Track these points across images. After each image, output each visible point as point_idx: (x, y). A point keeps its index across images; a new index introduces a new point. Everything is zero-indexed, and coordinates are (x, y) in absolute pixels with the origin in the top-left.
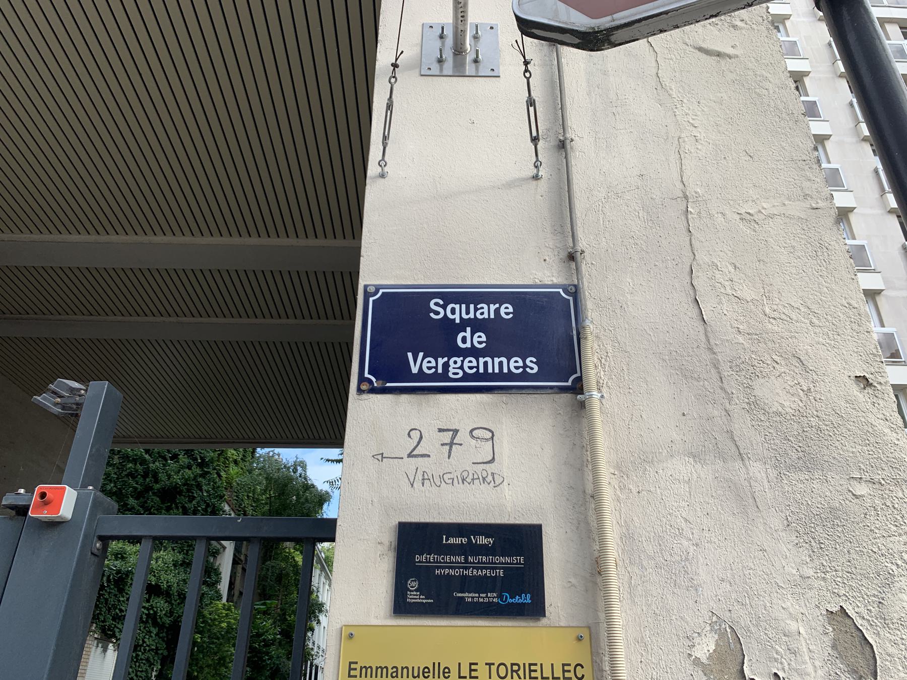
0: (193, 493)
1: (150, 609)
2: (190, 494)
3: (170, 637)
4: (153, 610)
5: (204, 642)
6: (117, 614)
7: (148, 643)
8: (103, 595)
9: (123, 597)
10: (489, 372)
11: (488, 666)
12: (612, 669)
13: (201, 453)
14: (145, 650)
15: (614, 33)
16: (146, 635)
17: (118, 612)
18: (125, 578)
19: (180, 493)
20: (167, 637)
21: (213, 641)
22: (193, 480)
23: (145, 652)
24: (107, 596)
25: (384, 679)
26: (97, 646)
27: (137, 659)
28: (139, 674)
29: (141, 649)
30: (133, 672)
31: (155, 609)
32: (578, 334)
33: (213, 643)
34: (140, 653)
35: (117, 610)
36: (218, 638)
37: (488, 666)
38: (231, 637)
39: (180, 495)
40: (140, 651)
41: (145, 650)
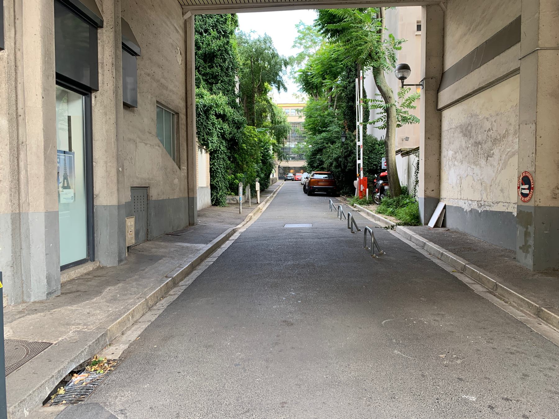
0: (224, 56)
2: (223, 57)
4: (223, 130)
5: (248, 149)
6: (208, 132)
7: (222, 149)
11: (404, 87)
12: (389, 51)
13: (222, 28)
14: (221, 153)
18: (353, 105)
19: (216, 56)
20: (228, 146)
22: (223, 47)
24: (202, 121)
27: (218, 158)
28: (220, 166)
30: (217, 165)
31: (224, 130)
35: (207, 130)
36: (255, 147)
37: (404, 87)
39: (217, 58)
40: (219, 153)
41: (221, 153)
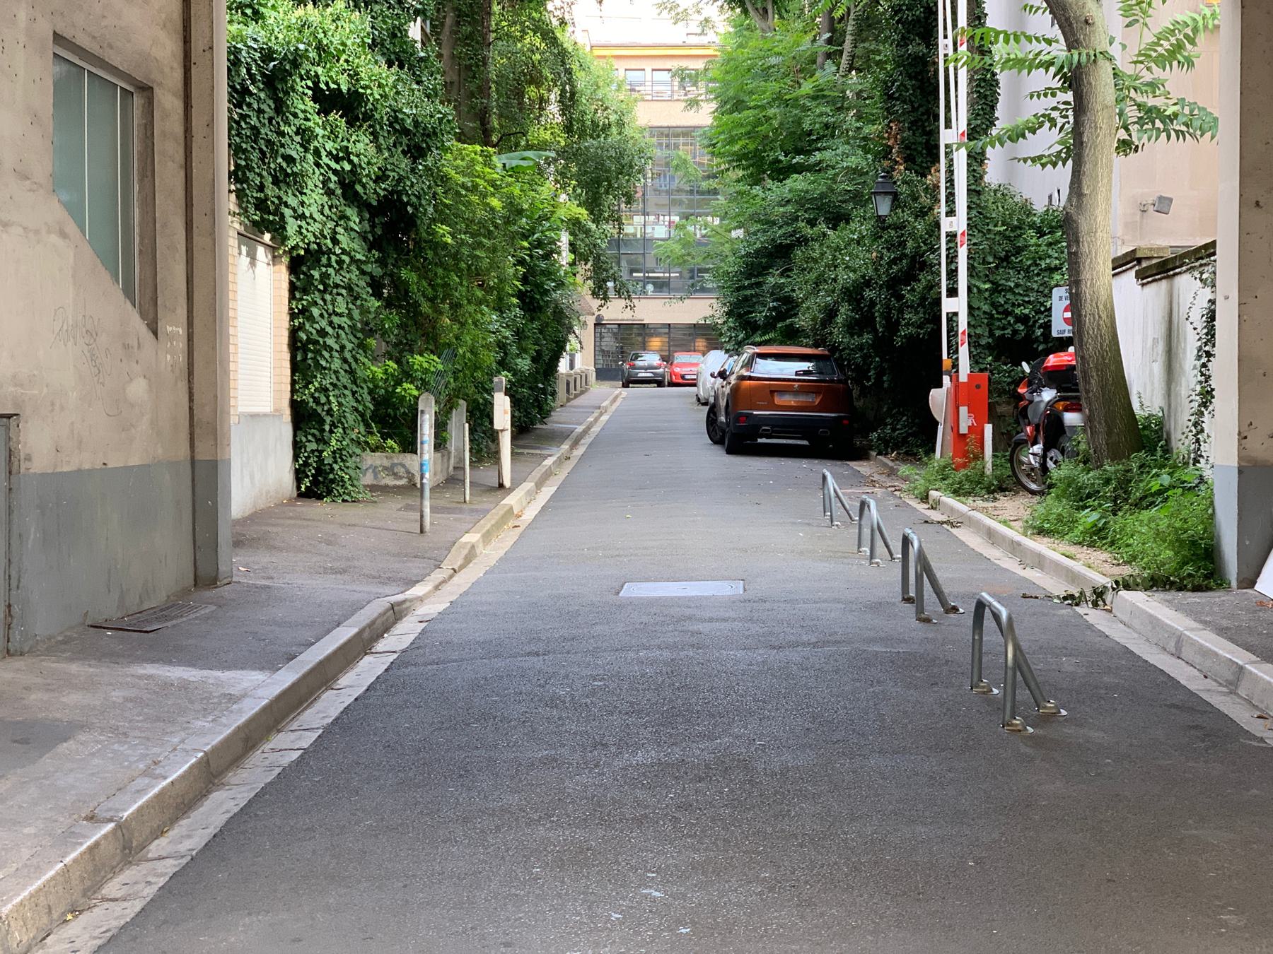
1: (343, 158)
3: (379, 231)
4: (350, 162)
8: (243, 117)
9: (288, 123)
10: (966, 408)
14: (340, 262)
15: (759, 655)
16: (337, 225)
17: (284, 165)
21: (481, 242)
23: (341, 268)
25: (1030, 4)
26: (252, 256)
28: (336, 320)
29: (329, 259)
30: (321, 315)
31: (355, 159)
32: (312, 703)
33: (480, 245)
34: (331, 271)
35: (280, 160)
36: (489, 235)
38: (517, 233)
40: (329, 265)
41: (340, 262)
